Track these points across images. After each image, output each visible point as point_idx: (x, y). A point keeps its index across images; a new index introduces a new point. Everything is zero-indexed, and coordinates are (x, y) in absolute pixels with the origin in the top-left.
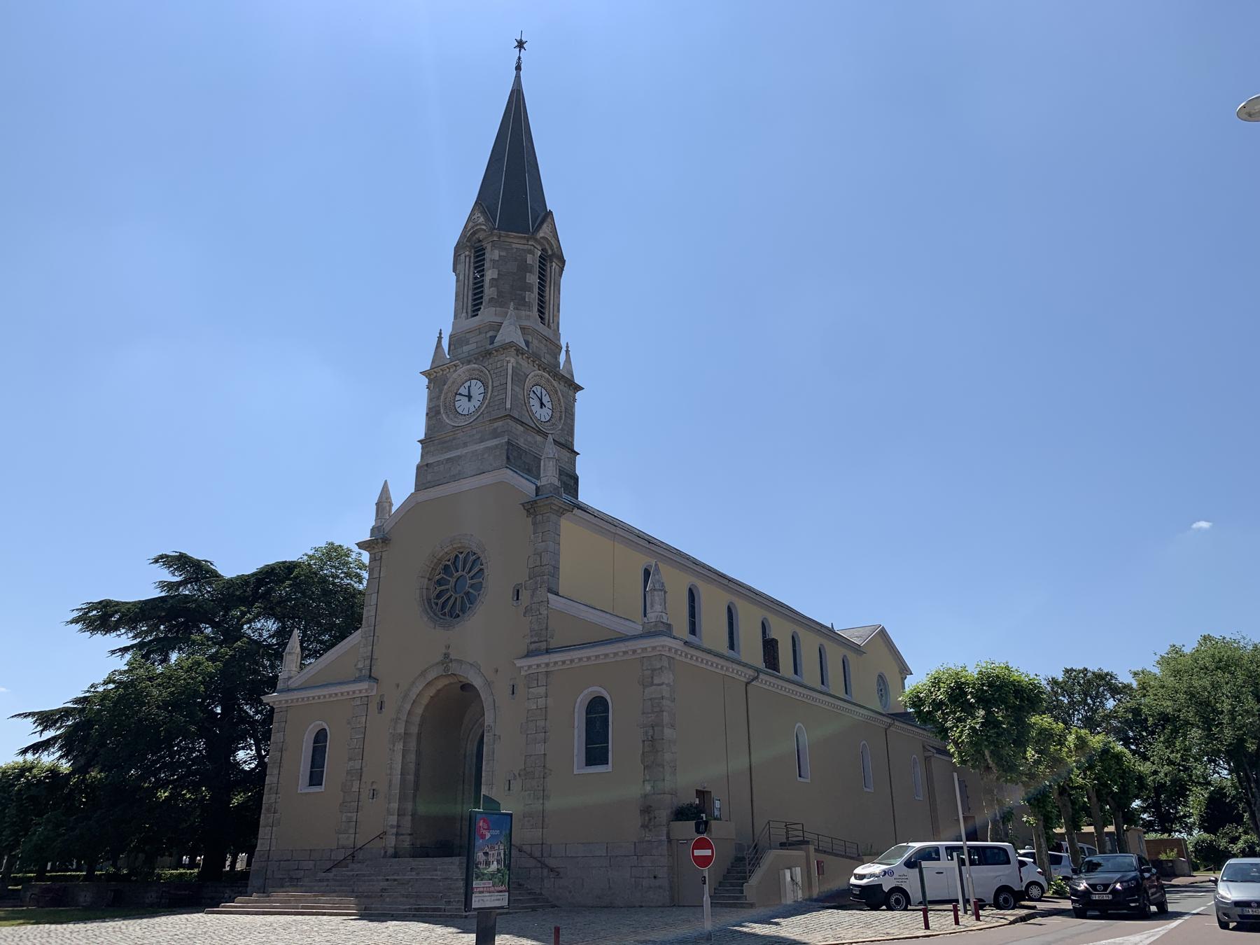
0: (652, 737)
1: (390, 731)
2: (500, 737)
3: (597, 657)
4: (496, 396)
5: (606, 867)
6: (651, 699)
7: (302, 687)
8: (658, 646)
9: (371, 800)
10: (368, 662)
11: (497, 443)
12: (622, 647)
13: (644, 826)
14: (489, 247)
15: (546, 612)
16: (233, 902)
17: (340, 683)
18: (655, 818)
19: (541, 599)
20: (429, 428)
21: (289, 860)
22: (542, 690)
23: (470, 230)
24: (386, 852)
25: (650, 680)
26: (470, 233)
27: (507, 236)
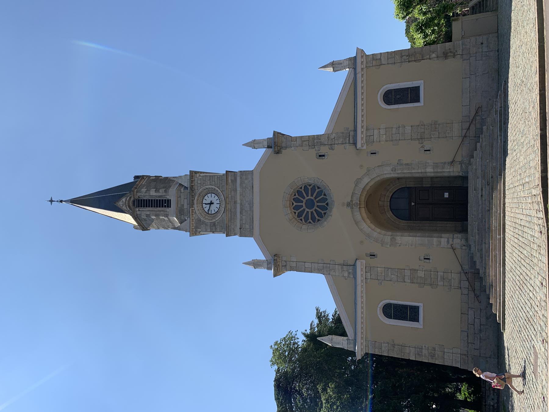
1: (388, 246)
2: (399, 160)
5: (476, 77)
6: (388, 59)
7: (354, 329)
8: (361, 347)
9: (431, 261)
12: (359, 85)
14: (139, 194)
16: (500, 323)
17: (355, 304)
18: (450, 49)
21: (468, 334)
22: (376, 132)
23: (127, 208)
24: (464, 245)
25: (378, 61)
26: (128, 208)
27: (137, 185)
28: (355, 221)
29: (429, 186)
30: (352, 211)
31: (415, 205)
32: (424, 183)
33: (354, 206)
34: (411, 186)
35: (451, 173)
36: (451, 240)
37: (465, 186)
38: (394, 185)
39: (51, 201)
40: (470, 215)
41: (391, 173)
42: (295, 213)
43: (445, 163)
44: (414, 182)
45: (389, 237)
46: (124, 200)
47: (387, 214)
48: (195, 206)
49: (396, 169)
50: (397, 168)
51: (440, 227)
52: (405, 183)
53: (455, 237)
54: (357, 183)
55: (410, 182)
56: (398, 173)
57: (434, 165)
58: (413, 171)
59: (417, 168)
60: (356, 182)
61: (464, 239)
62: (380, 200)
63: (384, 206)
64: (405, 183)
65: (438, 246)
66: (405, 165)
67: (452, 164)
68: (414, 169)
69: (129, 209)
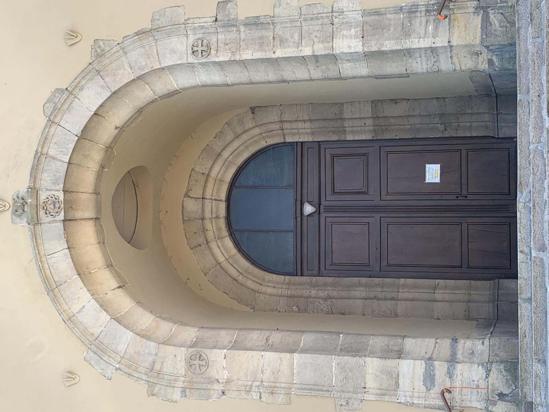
1: (177, 395)
24: (501, 396)
28: (46, 280)
29: (369, 137)
30: (35, 236)
31: (318, 212)
32: (346, 124)
33: (42, 213)
34: (301, 140)
35: (442, 57)
36: (440, 368)
37: (504, 132)
38: (237, 137)
40: (526, 250)
41: (191, 66)
43: (412, 11)
44: (310, 121)
45: (182, 353)
47: (217, 251)
49: (209, 47)
50: (214, 39)
51: (406, 300)
52: (277, 127)
53: (459, 356)
54: (54, 109)
55: (296, 121)
56: (220, 65)
57: (367, 19)
58: (280, 53)
59: (296, 36)
60: (50, 106)
61: (502, 367)
62: (187, 195)
63: (203, 219)
64: (277, 127)
65: (387, 398)
66: (246, 25)
67: (444, 12)
68: (283, 42)
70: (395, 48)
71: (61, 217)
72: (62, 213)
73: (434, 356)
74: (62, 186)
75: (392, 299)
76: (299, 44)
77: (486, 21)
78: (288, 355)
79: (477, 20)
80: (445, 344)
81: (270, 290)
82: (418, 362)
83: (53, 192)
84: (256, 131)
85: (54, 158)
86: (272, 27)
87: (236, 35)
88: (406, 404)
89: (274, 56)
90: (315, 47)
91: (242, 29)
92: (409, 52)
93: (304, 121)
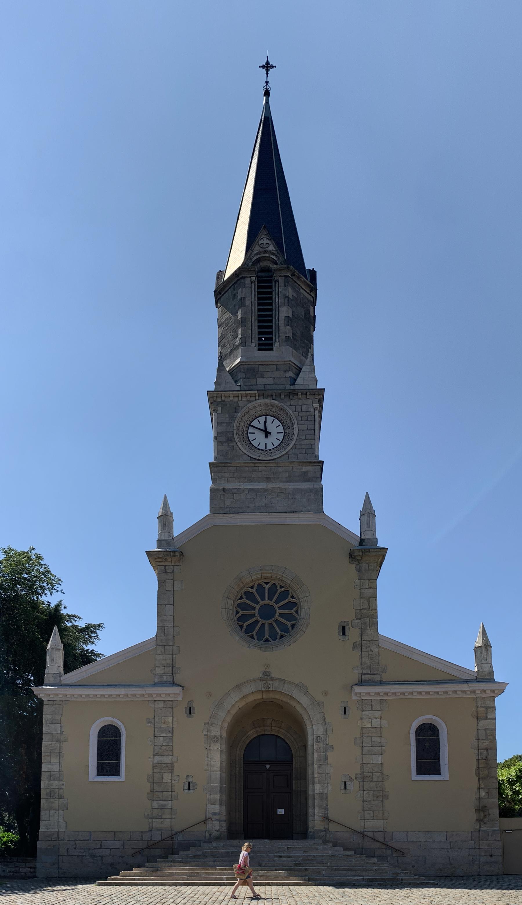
0: (486, 757)
1: (205, 733)
2: (332, 747)
3: (428, 693)
4: (303, 440)
9: (187, 791)
10: (169, 669)
11: (312, 487)
13: (479, 821)
14: (282, 281)
15: (377, 650)
18: (489, 815)
19: (372, 638)
20: (218, 453)
22: (377, 714)
23: (257, 254)
24: (210, 835)
27: (299, 278)
29: (294, 789)
31: (267, 770)
33: (264, 682)
36: (217, 817)
39: (267, 67)
40: (253, 842)
41: (313, 735)
42: (252, 587)
43: (327, 809)
45: (218, 734)
46: (271, 248)
47: (252, 731)
48: (262, 401)
49: (319, 742)
53: (221, 822)
57: (325, 795)
58: (316, 766)
59: (320, 772)
62: (273, 720)
65: (208, 801)
66: (325, 755)
68: (319, 767)
69: (253, 260)
70: (315, 804)
71: (263, 690)
72: (265, 690)
73: (221, 815)
74: (274, 690)
75: (236, 797)
76: (318, 773)
77: (322, 831)
78: (219, 769)
79: (322, 828)
80: (224, 818)
81: (238, 752)
82: (219, 810)
83: (272, 686)
84: (297, 747)
85: (284, 686)
86: (324, 764)
87: (322, 752)
88: (206, 807)
89: (315, 764)
90: (317, 778)
91: (324, 754)
92: (314, 808)
93: (300, 765)
